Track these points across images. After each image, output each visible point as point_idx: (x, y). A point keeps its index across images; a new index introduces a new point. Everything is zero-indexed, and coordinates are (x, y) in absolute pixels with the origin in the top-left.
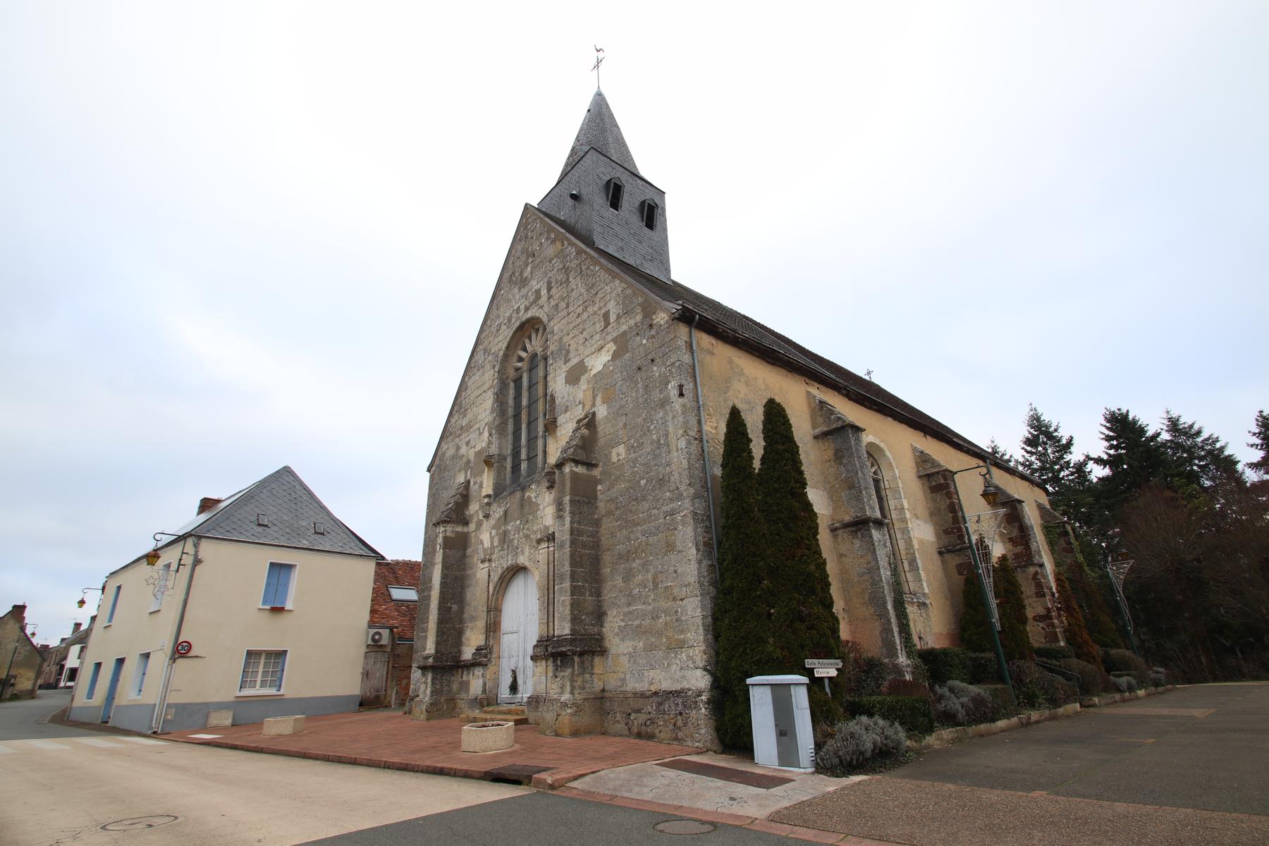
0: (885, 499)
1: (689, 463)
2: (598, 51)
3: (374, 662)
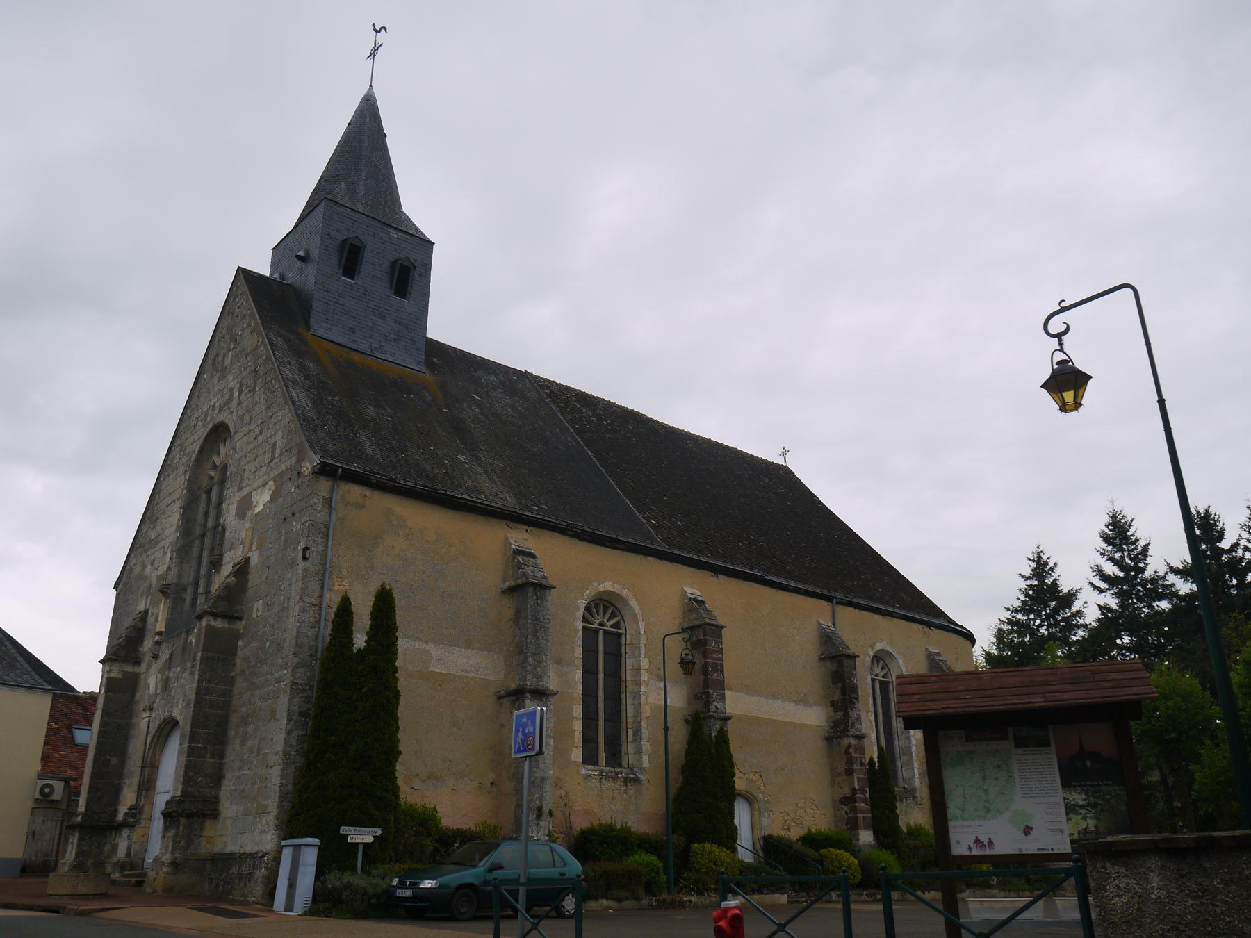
0: (623, 657)
1: (298, 632)
2: (377, 31)
3: (44, 820)
